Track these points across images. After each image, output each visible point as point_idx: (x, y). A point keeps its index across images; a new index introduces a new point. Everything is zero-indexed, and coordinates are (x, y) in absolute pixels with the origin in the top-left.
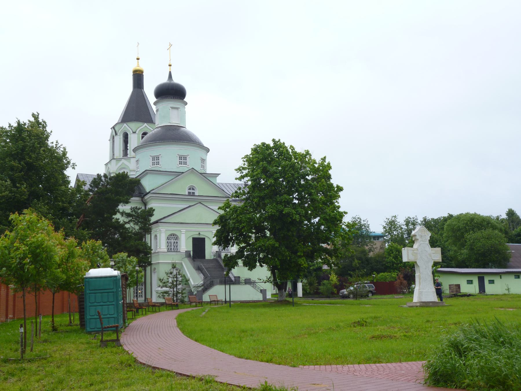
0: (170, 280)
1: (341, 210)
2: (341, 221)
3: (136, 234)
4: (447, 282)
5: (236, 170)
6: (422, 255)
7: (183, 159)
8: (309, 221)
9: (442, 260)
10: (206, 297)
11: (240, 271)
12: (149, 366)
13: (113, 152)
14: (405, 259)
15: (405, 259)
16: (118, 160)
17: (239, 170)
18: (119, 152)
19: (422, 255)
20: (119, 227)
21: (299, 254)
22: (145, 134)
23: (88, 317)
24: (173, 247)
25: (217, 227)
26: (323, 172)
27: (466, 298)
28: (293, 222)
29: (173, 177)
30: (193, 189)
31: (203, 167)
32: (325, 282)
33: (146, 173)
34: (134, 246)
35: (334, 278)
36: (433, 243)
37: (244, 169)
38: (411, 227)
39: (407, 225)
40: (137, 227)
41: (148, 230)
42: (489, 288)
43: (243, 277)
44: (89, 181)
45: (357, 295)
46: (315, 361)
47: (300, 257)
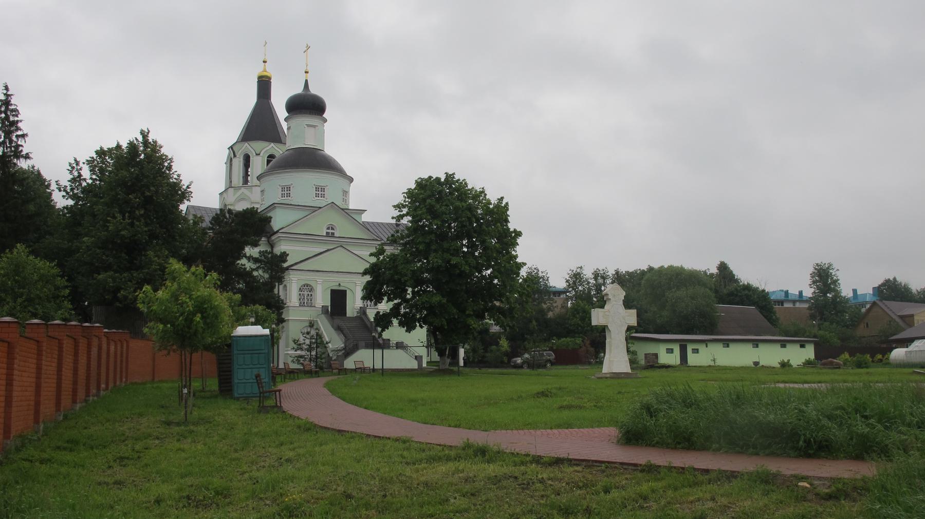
0: (308, 342)
1: (519, 260)
2: (518, 274)
3: (265, 284)
4: (643, 350)
5: (394, 206)
6: (615, 317)
7: (320, 191)
8: (480, 272)
9: (638, 323)
10: (349, 363)
11: (395, 332)
12: (333, 429)
13: (230, 178)
14: (594, 322)
15: (594, 322)
16: (237, 188)
17: (398, 207)
18: (238, 179)
19: (615, 317)
20: (245, 275)
21: (467, 312)
22: (271, 157)
23: (236, 381)
24: (306, 299)
25: (368, 278)
26: (500, 213)
27: (664, 369)
28: (462, 275)
29: (307, 213)
30: (332, 229)
31: (345, 200)
32: (494, 347)
33: (273, 207)
34: (264, 299)
35: (504, 344)
36: (628, 304)
37: (404, 206)
38: (601, 281)
39: (596, 278)
40: (266, 276)
41: (280, 280)
42: (692, 359)
43: (394, 340)
44: (208, 219)
45: (532, 365)
46: (506, 427)
47: (469, 316)
